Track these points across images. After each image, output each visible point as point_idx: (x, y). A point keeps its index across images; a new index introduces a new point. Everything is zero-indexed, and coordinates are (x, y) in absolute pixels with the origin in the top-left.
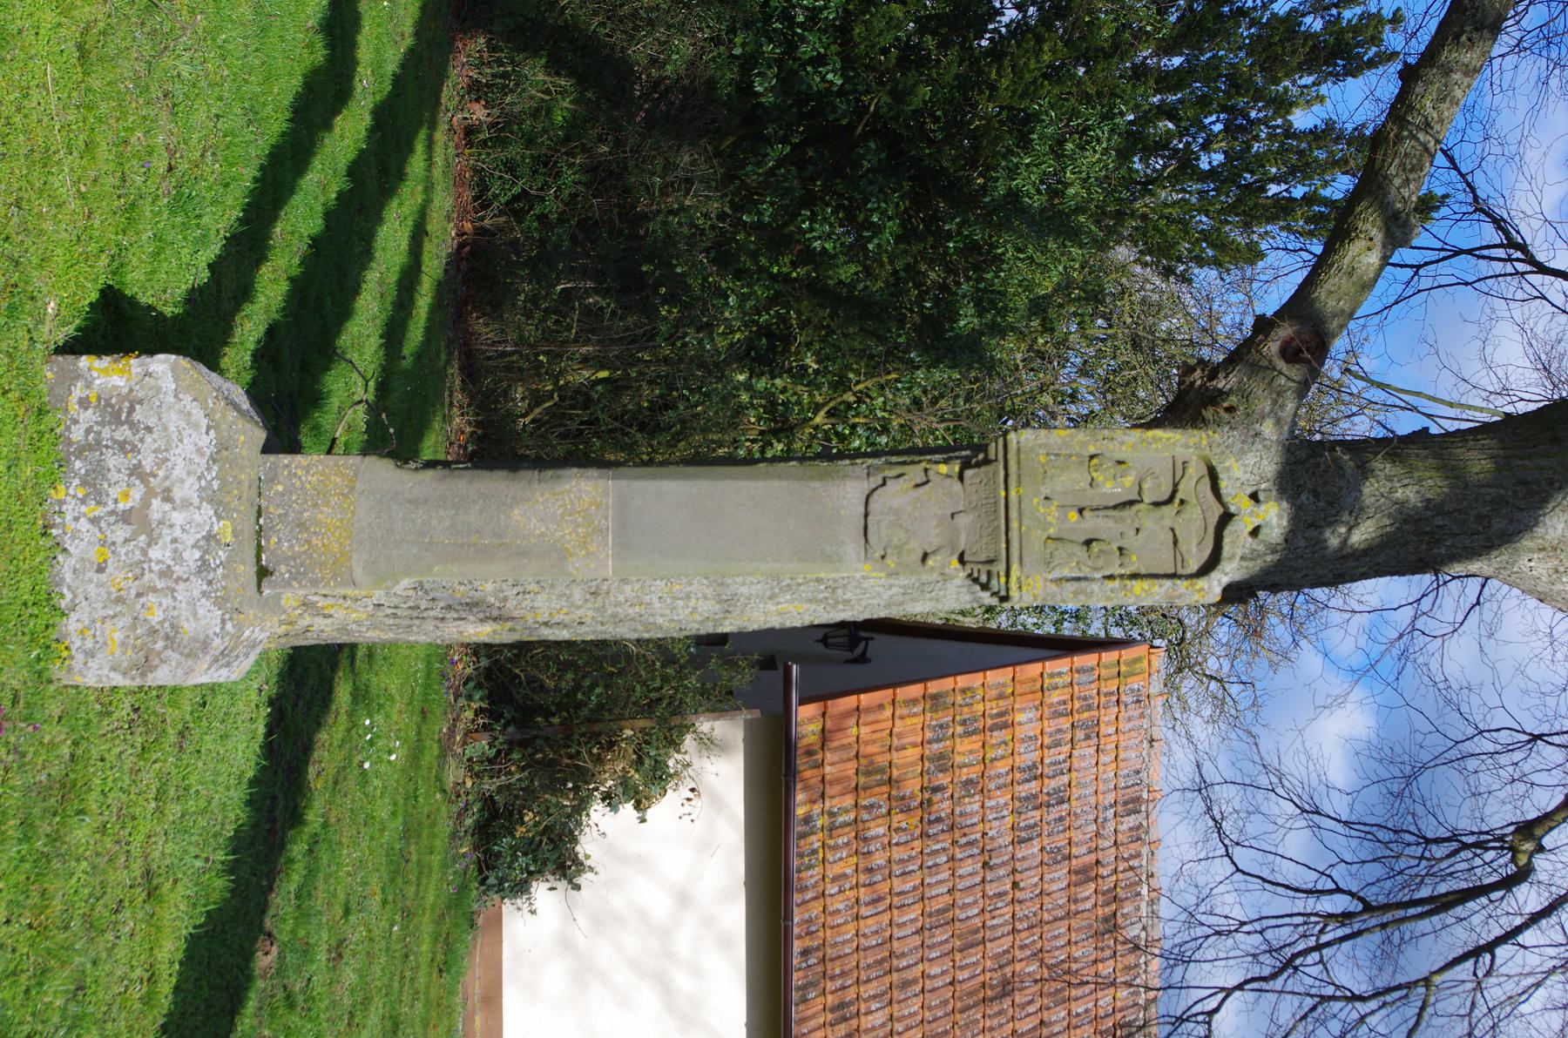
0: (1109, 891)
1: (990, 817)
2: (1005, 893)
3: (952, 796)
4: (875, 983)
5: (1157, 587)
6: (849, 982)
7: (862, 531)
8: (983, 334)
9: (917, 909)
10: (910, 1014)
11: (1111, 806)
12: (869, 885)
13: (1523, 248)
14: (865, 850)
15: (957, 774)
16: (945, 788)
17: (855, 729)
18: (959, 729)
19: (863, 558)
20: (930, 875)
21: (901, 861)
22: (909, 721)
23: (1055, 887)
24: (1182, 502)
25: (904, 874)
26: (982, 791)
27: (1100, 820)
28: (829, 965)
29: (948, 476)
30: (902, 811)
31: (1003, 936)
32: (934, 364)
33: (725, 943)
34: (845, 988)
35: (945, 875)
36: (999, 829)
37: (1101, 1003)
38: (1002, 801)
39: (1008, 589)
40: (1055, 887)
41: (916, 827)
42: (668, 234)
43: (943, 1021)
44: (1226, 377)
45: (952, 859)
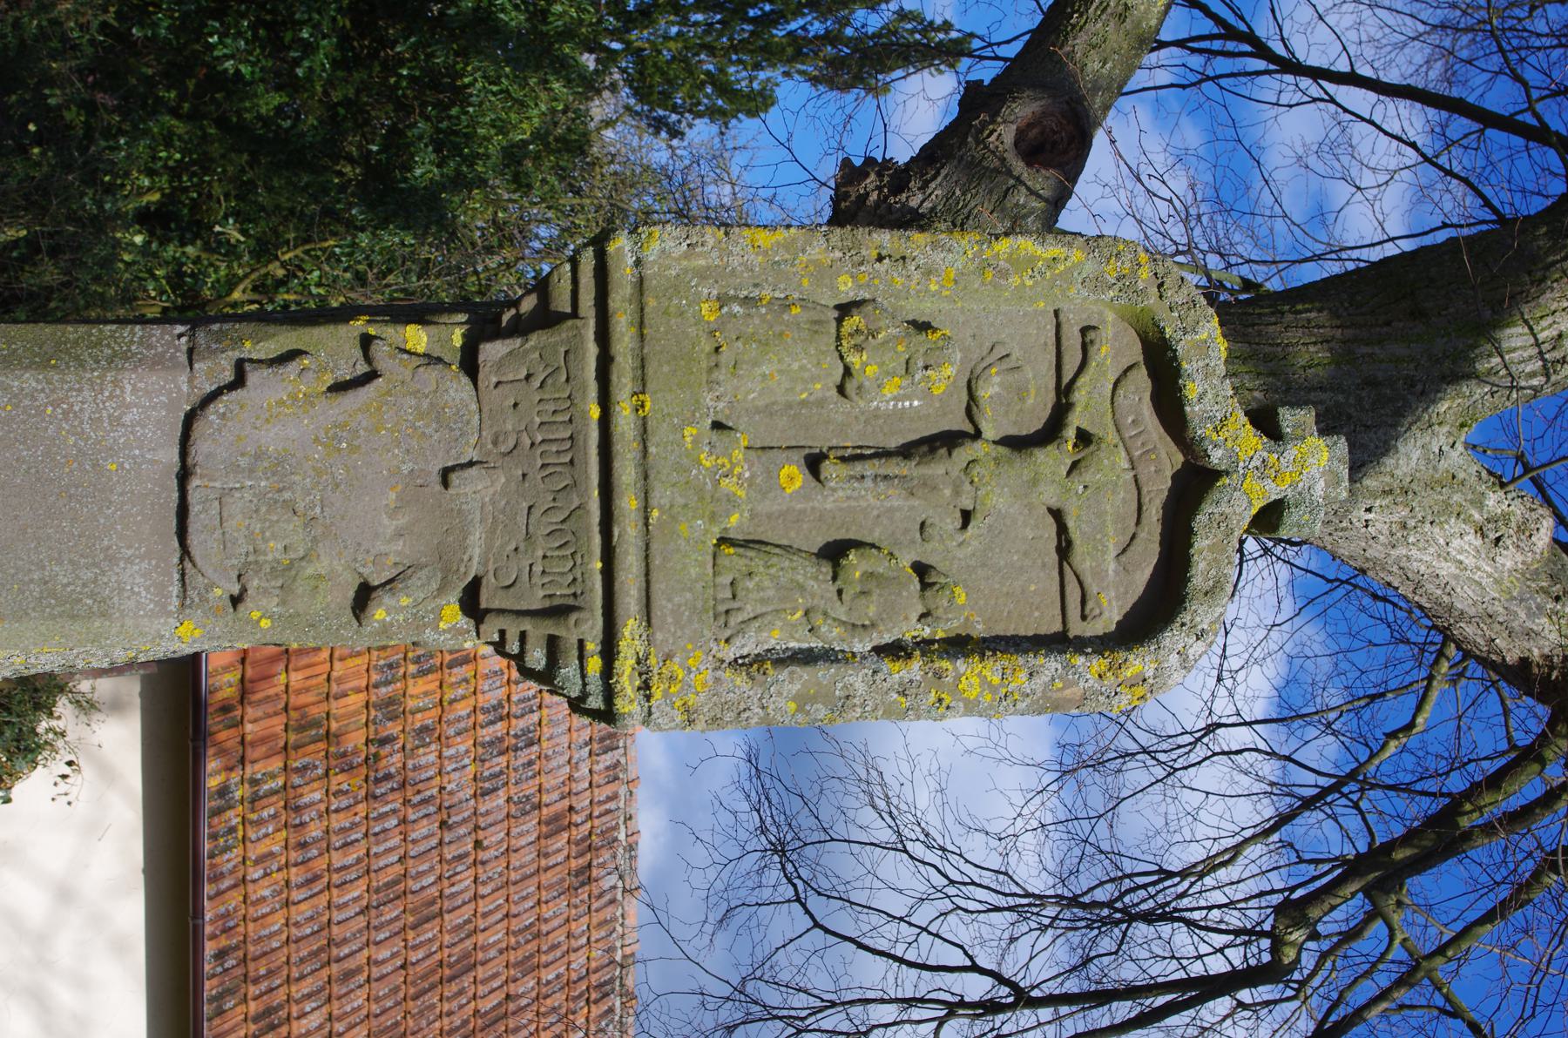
0: (583, 840)
1: (449, 769)
2: (467, 855)
3: (404, 748)
4: (310, 980)
5: (1022, 675)
6: (278, 982)
7: (173, 523)
8: (444, 188)
9: (361, 887)
10: (353, 1009)
11: (586, 744)
12: (303, 863)
13: (1250, 38)
14: (297, 821)
15: (410, 721)
16: (395, 739)
17: (284, 676)
18: (412, 668)
19: (175, 602)
20: (378, 843)
21: (343, 830)
22: (350, 663)
23: (523, 842)
24: (1084, 438)
25: (346, 845)
26: (439, 738)
27: (574, 761)
28: (252, 966)
29: (431, 359)
30: (343, 771)
31: (464, 903)
32: (383, 223)
33: (119, 947)
34: (272, 990)
35: (395, 841)
36: (460, 784)
37: (573, 966)
38: (462, 748)
39: (609, 694)
40: (523, 842)
41: (360, 787)
42: (22, 42)
43: (392, 1013)
44: (923, 188)
45: (404, 821)
